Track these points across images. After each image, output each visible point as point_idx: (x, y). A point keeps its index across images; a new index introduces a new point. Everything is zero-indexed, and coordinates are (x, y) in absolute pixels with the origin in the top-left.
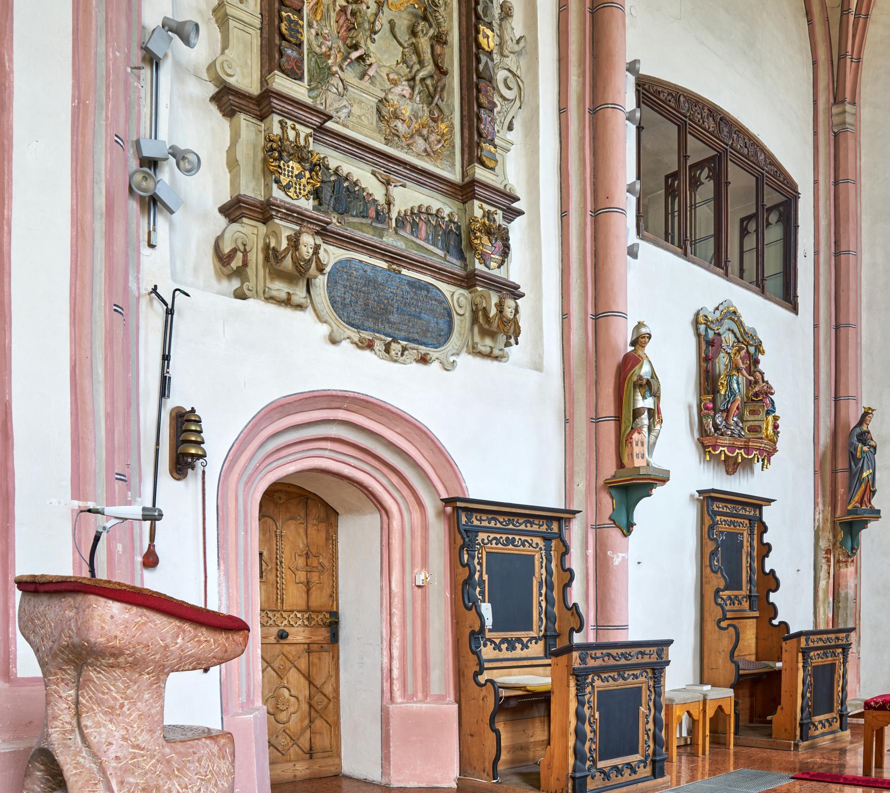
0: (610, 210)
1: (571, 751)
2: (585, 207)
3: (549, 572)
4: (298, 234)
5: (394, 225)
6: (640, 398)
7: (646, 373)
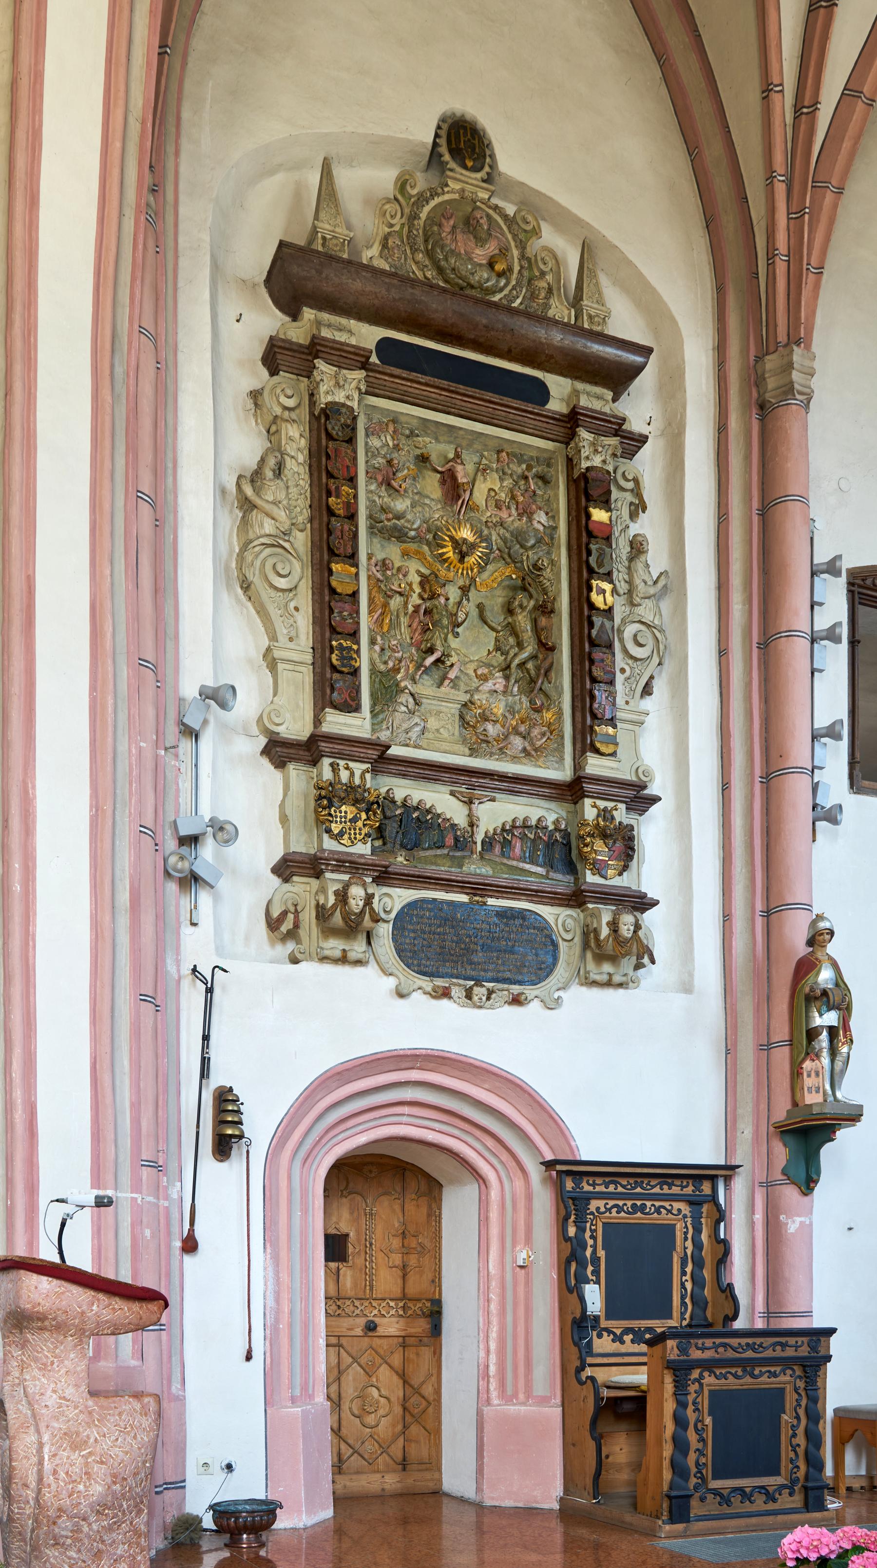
0: (784, 772)
1: (666, 1464)
2: (752, 774)
3: (698, 1245)
4: (347, 886)
5: (479, 848)
6: (816, 1014)
7: (826, 981)
